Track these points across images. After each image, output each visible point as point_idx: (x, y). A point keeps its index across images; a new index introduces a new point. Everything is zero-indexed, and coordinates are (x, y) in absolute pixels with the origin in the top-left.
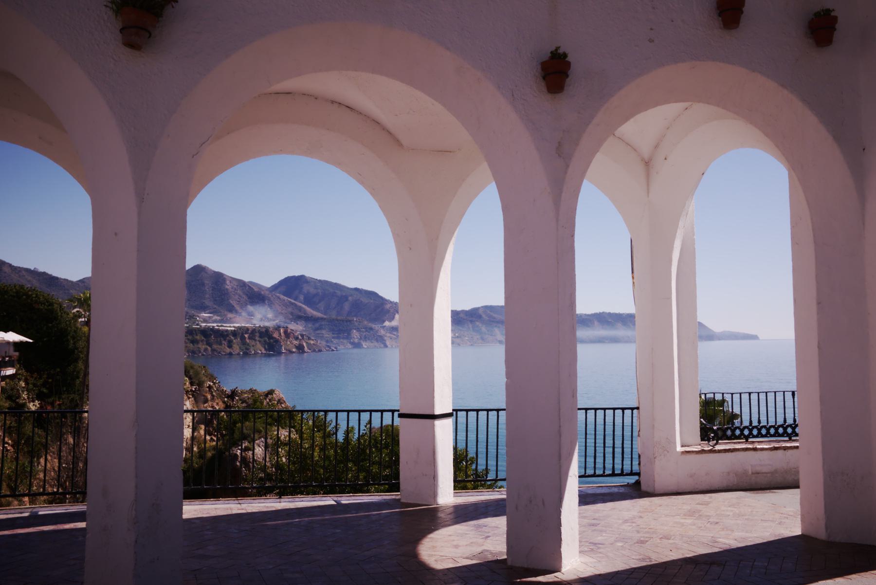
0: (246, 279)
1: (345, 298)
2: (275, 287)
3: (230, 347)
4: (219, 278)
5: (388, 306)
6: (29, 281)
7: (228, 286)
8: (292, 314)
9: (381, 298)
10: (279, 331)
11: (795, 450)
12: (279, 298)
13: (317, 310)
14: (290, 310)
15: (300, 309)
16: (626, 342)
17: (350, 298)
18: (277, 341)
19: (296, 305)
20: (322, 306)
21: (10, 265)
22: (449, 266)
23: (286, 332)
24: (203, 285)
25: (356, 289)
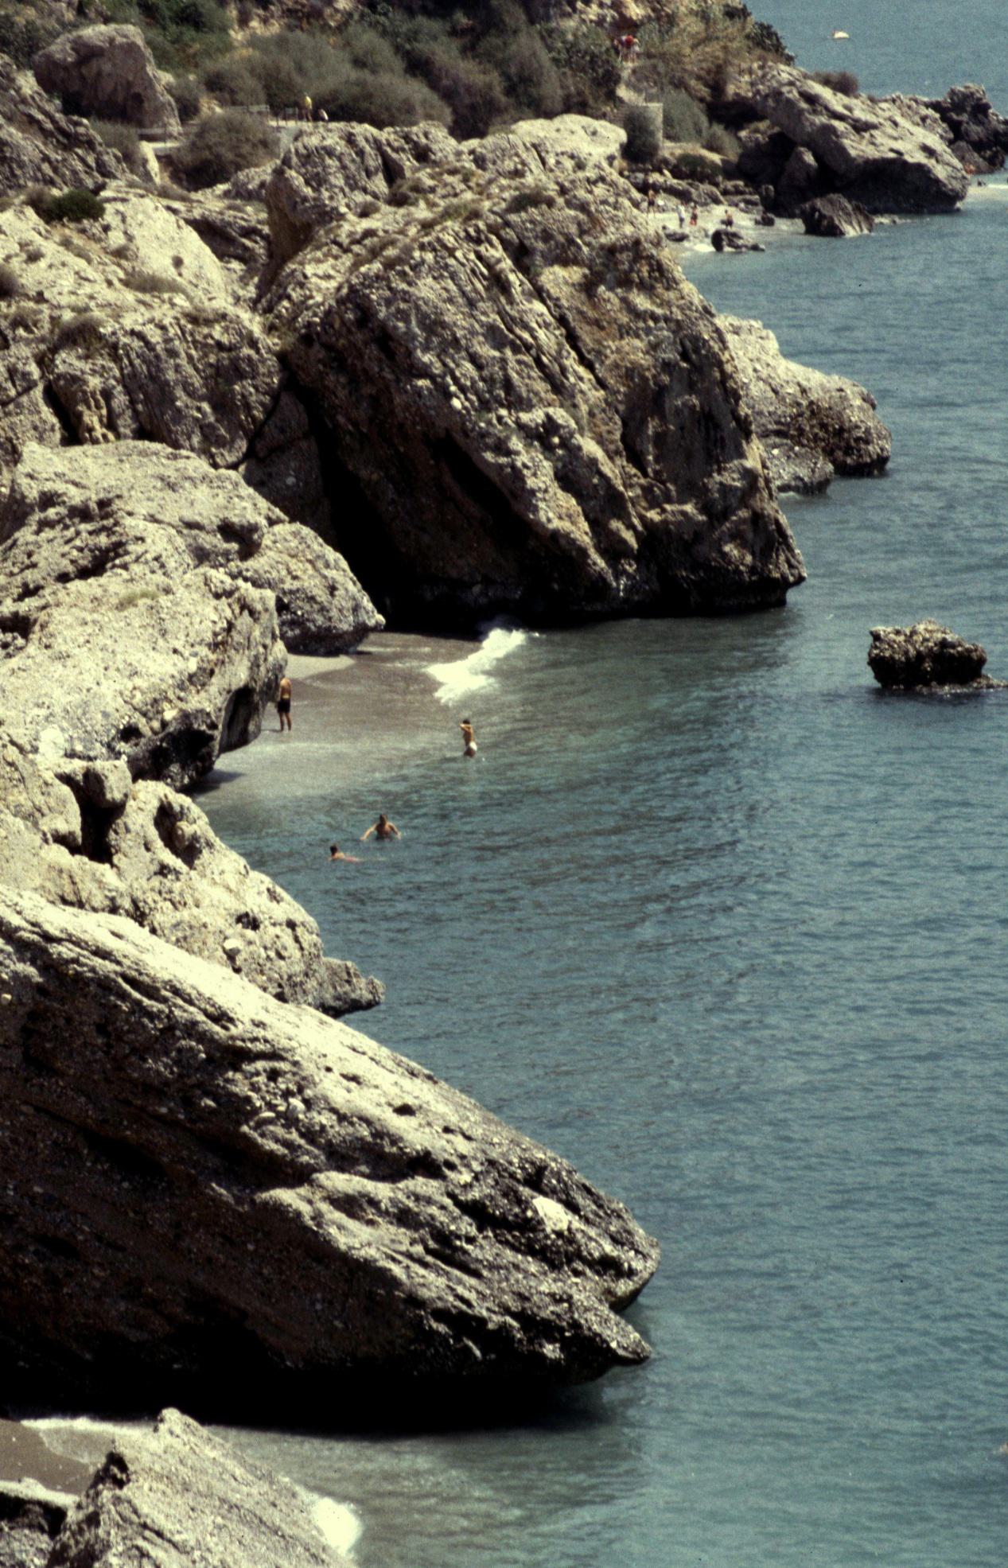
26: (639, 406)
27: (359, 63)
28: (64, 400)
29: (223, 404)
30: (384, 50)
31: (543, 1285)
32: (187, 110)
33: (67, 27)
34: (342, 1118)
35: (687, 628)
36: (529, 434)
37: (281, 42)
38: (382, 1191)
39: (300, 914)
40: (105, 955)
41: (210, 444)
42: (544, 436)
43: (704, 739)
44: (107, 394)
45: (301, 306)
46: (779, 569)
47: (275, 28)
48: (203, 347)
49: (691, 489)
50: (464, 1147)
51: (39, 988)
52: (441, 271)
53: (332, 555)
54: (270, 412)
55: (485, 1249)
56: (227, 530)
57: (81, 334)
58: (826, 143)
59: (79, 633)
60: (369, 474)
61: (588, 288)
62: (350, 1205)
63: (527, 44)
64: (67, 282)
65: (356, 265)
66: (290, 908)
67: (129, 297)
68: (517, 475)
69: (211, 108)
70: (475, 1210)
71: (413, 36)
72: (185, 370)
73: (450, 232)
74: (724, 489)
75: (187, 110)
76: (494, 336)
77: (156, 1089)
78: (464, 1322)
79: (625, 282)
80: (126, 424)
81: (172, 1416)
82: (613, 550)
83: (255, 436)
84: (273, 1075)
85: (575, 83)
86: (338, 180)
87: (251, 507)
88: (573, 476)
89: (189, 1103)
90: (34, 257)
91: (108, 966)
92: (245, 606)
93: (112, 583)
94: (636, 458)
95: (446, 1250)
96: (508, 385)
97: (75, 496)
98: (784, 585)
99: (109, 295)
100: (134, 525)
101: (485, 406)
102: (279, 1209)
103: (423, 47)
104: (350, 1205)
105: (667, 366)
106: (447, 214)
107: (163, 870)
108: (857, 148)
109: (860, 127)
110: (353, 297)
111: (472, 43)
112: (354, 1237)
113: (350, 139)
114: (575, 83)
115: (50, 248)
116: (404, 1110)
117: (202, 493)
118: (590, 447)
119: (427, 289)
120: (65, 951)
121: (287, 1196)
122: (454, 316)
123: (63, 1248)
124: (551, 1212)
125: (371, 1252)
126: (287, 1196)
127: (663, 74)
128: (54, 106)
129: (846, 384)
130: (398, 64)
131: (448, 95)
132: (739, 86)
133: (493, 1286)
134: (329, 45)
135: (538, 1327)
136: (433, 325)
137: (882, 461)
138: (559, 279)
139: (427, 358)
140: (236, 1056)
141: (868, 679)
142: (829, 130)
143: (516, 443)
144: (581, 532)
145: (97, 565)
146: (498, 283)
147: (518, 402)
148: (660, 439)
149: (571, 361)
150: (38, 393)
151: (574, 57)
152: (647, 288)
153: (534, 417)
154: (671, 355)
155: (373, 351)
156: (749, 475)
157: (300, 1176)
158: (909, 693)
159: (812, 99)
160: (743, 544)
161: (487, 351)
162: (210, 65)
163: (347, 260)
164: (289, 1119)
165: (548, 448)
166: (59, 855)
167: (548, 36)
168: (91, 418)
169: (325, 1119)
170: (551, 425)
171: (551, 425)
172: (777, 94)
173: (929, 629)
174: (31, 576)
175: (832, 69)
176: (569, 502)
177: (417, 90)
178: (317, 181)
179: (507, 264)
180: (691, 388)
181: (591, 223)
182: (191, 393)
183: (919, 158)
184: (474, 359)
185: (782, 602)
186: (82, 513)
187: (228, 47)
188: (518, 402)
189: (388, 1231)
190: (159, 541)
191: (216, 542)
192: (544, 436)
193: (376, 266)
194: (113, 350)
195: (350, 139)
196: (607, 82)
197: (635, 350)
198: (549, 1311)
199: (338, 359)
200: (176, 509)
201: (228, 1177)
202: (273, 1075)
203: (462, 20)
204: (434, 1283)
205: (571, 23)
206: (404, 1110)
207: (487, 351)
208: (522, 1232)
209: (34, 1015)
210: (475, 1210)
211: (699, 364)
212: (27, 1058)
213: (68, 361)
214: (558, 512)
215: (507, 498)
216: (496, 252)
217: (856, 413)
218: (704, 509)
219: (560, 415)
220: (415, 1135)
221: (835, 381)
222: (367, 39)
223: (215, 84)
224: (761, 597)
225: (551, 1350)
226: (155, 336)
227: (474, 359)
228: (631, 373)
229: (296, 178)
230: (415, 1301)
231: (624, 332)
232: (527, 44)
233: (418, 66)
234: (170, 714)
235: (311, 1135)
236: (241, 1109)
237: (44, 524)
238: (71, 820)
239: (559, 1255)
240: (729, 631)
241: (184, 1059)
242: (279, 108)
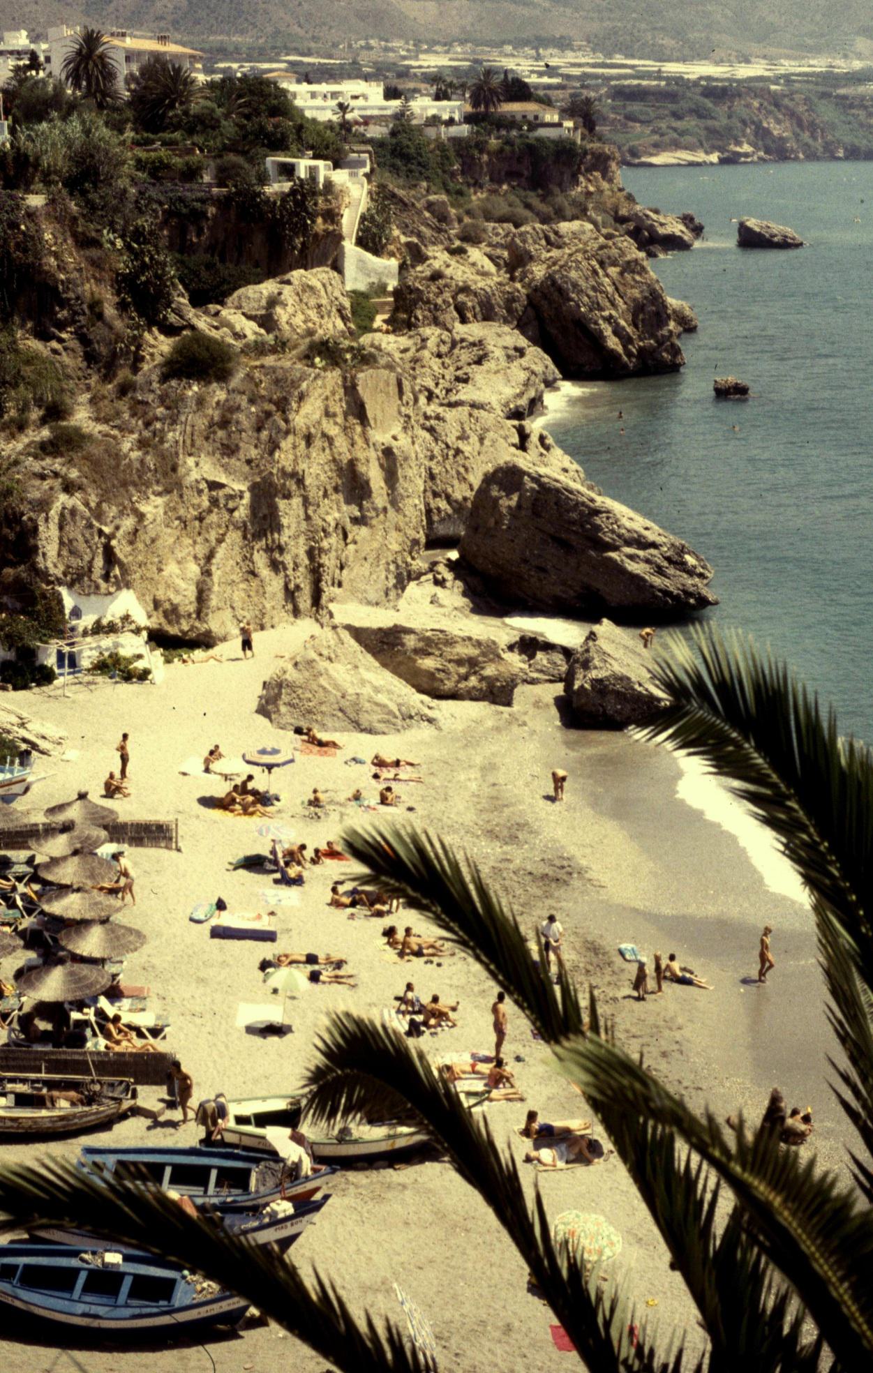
26: (637, 310)
27: (510, 205)
28: (461, 310)
29: (510, 310)
30: (518, 201)
31: (689, 581)
32: (460, 220)
33: (424, 196)
34: (629, 531)
35: (652, 380)
36: (605, 319)
37: (487, 199)
38: (641, 553)
39: (580, 469)
40: (557, 481)
41: (506, 321)
42: (609, 319)
43: (654, 410)
44: (474, 307)
45: (533, 279)
46: (678, 360)
47: (484, 195)
48: (503, 292)
49: (653, 336)
50: (664, 540)
51: (538, 492)
52: (577, 269)
53: (546, 356)
54: (524, 312)
55: (671, 571)
56: (516, 349)
57: (465, 289)
58: (651, 229)
59: (483, 382)
60: (554, 331)
61: (621, 274)
62: (632, 557)
63: (560, 199)
64: (460, 273)
65: (549, 267)
66: (575, 466)
67: (479, 278)
68: (601, 332)
69: (467, 220)
70: (668, 559)
71: (526, 197)
72: (498, 300)
73: (580, 257)
74: (663, 336)
75: (460, 220)
76: (594, 289)
77: (574, 523)
78: (666, 593)
79: (633, 272)
80: (479, 317)
81: (605, 621)
82: (629, 354)
83: (519, 320)
84: (608, 518)
85: (575, 211)
86: (530, 241)
87: (522, 342)
88: (618, 332)
89: (582, 526)
90: (448, 266)
91: (558, 485)
92: (533, 373)
93: (487, 365)
94: (636, 326)
95: (660, 571)
96: (598, 304)
97: (471, 339)
98: (680, 365)
99: (472, 277)
100: (490, 348)
101: (591, 310)
102: (611, 559)
103: (529, 200)
104: (632, 557)
105: (646, 298)
106: (577, 251)
107: (541, 455)
108: (661, 231)
109: (662, 225)
110: (550, 277)
111: (543, 199)
112: (633, 567)
113: (534, 229)
114: (575, 211)
115: (453, 263)
116: (647, 529)
117: (508, 338)
118: (622, 323)
119: (573, 274)
120: (546, 480)
121: (613, 555)
122: (582, 283)
123: (542, 570)
124: (690, 560)
125: (638, 572)
126: (613, 555)
127: (599, 207)
128: (435, 220)
129: (684, 303)
130: (522, 206)
131: (538, 214)
132: (623, 212)
133: (673, 582)
134: (501, 199)
135: (688, 594)
136: (575, 285)
137: (695, 327)
138: (613, 271)
139: (573, 295)
140: (597, 512)
141: (713, 393)
142: (652, 226)
143: (601, 322)
144: (620, 349)
145: (479, 362)
146: (595, 272)
147: (601, 309)
148: (643, 320)
149: (617, 296)
150: (452, 308)
151: (574, 203)
152: (639, 274)
153: (606, 313)
154: (647, 294)
155: (556, 294)
156: (671, 332)
157: (616, 549)
158: (726, 399)
159: (647, 216)
160: (668, 353)
161: (592, 293)
162: (466, 207)
163: (545, 266)
164: (613, 531)
165: (610, 323)
166: (513, 450)
167: (566, 197)
168: (469, 315)
169: (623, 531)
170: (611, 316)
171: (611, 316)
172: (636, 214)
173: (732, 379)
174: (459, 364)
175: (654, 207)
176: (616, 340)
177: (527, 213)
178: (524, 241)
179: (597, 267)
180: (653, 304)
181: (623, 254)
182: (500, 306)
183: (679, 234)
184: (588, 296)
185: (678, 371)
186: (474, 344)
187: (471, 201)
188: (601, 309)
189: (647, 567)
190: (499, 353)
191: (512, 352)
192: (609, 319)
193: (557, 268)
194: (475, 294)
195: (534, 229)
196: (585, 210)
197: (636, 293)
198: (692, 589)
199: (545, 296)
200: (501, 342)
201: (595, 549)
202: (608, 518)
203: (540, 192)
204: (657, 581)
205: (573, 193)
206: (647, 529)
207: (592, 293)
208: (681, 565)
209: (536, 500)
210: (668, 559)
211: (655, 297)
212: (534, 513)
213: (461, 297)
214: (613, 343)
215: (598, 339)
216: (594, 263)
217: (688, 312)
218: (657, 341)
219: (614, 313)
220: (651, 536)
221: (680, 302)
222: (512, 198)
223: (468, 213)
224: (673, 368)
225: (692, 601)
226: (488, 290)
227: (588, 296)
228: (635, 300)
229: (518, 241)
230: (652, 586)
231: (632, 287)
232: (560, 199)
233: (528, 206)
234: (512, 406)
235: (620, 536)
236: (598, 528)
237: (462, 348)
238: (516, 440)
239: (691, 572)
240: (664, 380)
241: (581, 514)
242: (488, 219)
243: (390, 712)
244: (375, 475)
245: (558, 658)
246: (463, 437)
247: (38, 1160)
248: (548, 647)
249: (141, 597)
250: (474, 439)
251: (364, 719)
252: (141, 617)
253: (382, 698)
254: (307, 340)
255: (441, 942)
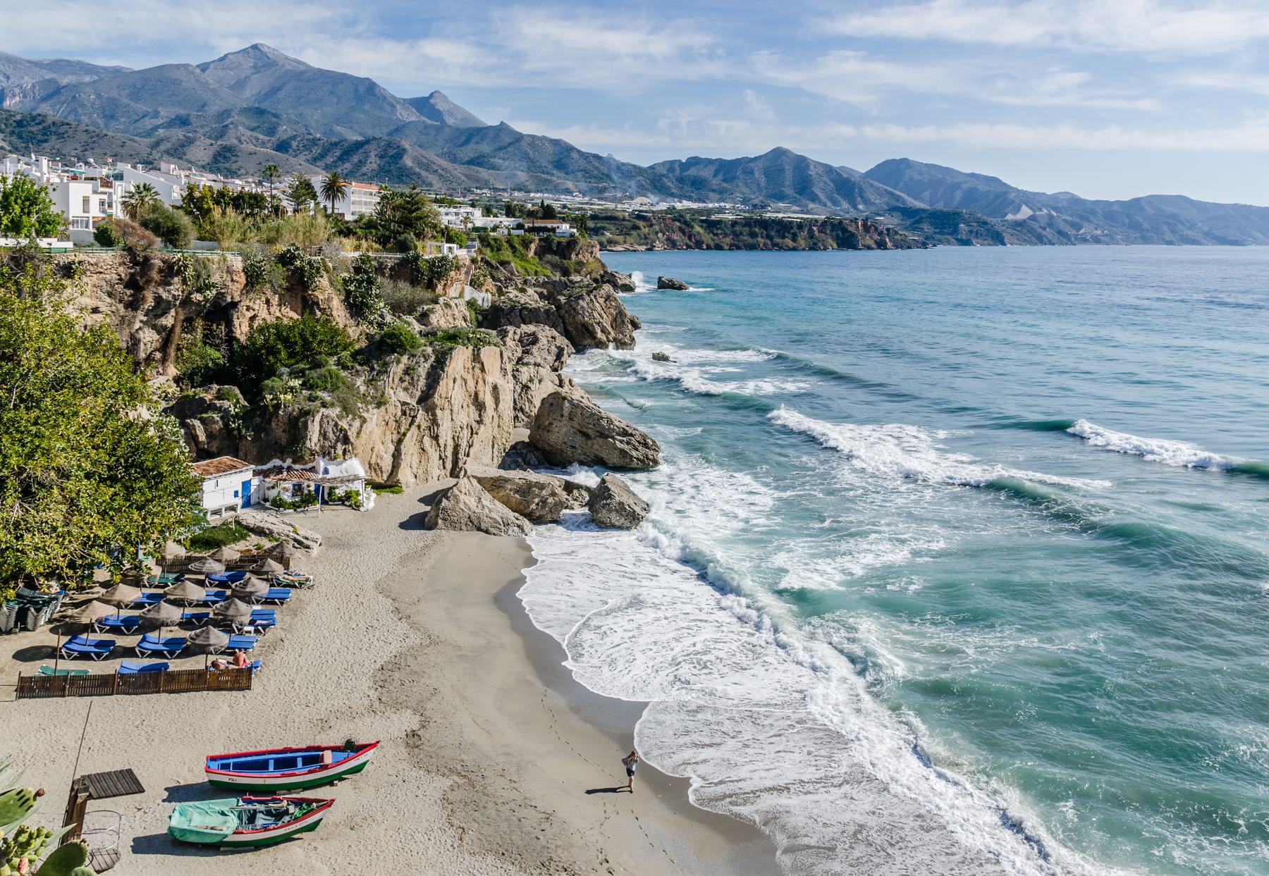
0: (835, 164)
1: (957, 186)
2: (870, 173)
3: (794, 240)
4: (801, 163)
5: (1012, 196)
6: (596, 168)
7: (812, 172)
8: (887, 204)
9: (1005, 185)
10: (857, 224)
11: (590, 789)
12: (872, 185)
13: (921, 200)
14: (886, 199)
15: (898, 198)
16: (1064, 237)
17: (964, 186)
18: (853, 235)
19: (893, 194)
20: (927, 194)
21: (578, 151)
22: (927, 133)
23: (864, 225)
24: (783, 170)
25: (973, 175)
42: (598, 323)
192: (598, 323)
243: (497, 522)
244: (488, 400)
245: (585, 494)
246: (531, 380)
247: (329, 804)
248: (579, 487)
249: (362, 463)
250: (536, 381)
251: (483, 526)
252: (361, 472)
253: (493, 515)
254: (236, 142)
255: (718, 740)
